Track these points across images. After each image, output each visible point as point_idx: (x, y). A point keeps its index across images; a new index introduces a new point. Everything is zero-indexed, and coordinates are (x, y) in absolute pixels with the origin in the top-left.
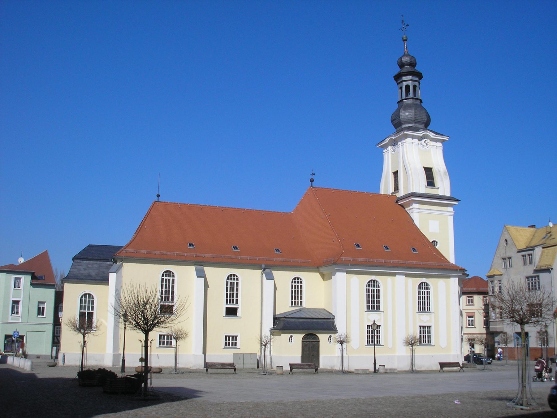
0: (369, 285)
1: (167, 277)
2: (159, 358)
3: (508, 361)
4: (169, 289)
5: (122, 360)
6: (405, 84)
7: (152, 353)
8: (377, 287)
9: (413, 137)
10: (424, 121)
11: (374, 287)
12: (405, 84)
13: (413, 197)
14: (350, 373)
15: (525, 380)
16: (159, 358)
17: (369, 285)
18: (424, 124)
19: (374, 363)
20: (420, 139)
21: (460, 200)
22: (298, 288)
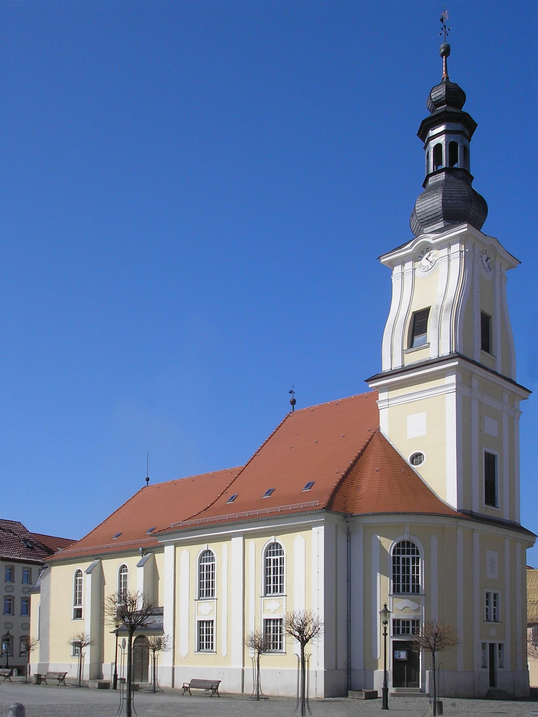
0: (399, 550)
1: (417, 557)
2: (72, 667)
3: (497, 687)
4: (403, 576)
5: (114, 675)
6: (433, 144)
7: (84, 663)
8: (413, 554)
9: (402, 262)
10: (439, 214)
11: (408, 553)
12: (433, 144)
13: (370, 382)
14: (266, 698)
15: (224, 699)
16: (71, 668)
17: (399, 550)
18: (442, 219)
19: (383, 689)
20: (417, 257)
21: (365, 381)
22: (408, 563)
